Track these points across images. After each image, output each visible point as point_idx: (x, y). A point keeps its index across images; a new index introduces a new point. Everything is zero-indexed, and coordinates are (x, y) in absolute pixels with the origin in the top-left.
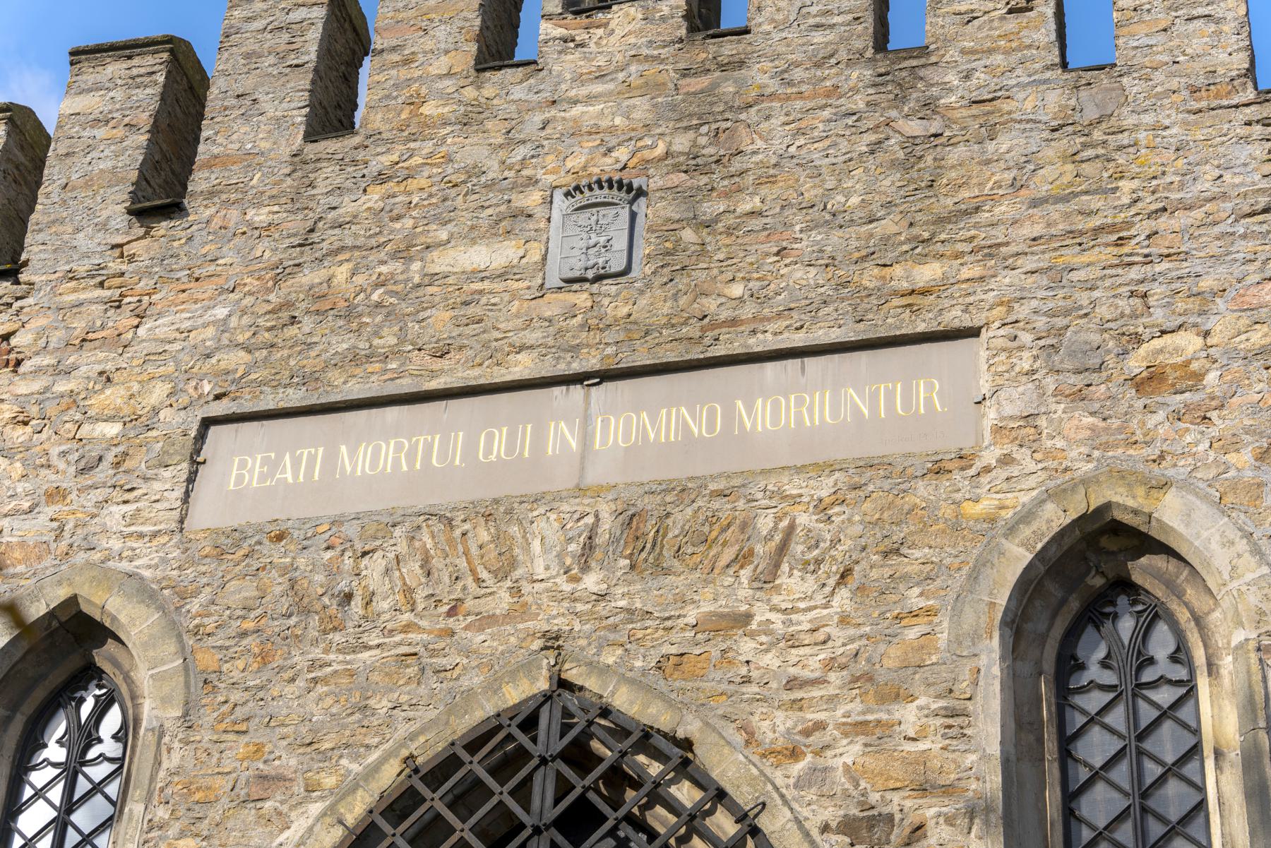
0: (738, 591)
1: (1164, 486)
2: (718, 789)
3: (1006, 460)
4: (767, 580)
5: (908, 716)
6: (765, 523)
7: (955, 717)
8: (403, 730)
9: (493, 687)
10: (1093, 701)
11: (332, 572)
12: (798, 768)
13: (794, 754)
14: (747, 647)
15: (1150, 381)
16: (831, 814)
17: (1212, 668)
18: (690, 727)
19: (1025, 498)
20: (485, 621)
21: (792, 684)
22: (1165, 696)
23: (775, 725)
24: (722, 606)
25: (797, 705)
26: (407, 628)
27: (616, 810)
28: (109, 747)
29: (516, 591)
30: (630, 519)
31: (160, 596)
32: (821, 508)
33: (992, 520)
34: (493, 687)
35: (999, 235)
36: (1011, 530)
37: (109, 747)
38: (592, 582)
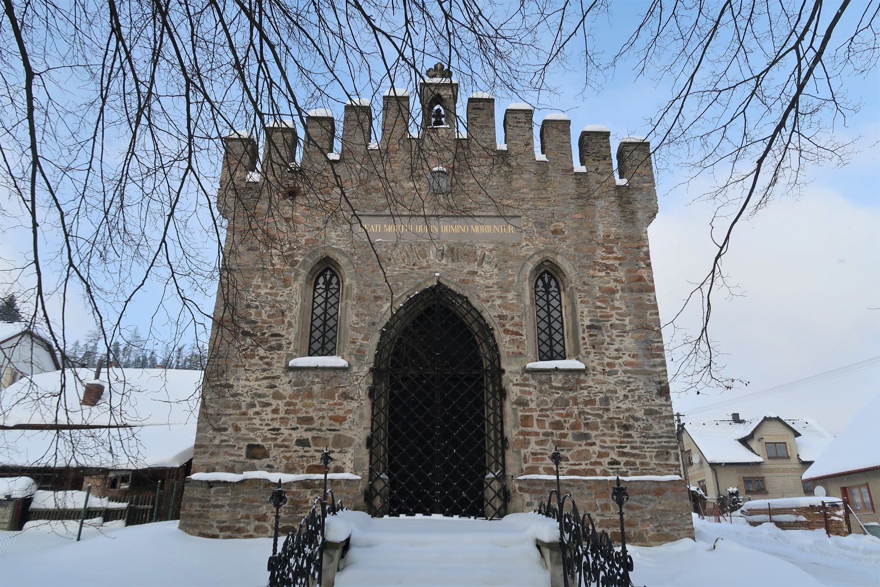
0: (474, 267)
1: (558, 254)
2: (767, 493)
3: (527, 245)
4: (480, 264)
5: (510, 296)
6: (479, 252)
7: (519, 296)
8: (406, 289)
9: (425, 281)
10: (320, 291)
11: (386, 252)
12: (489, 304)
13: (488, 301)
14: (477, 279)
15: (555, 232)
16: (496, 314)
17: (564, 290)
18: (466, 294)
19: (531, 253)
20: (421, 268)
21: (487, 287)
22: (334, 291)
23: (483, 295)
24: (472, 269)
25: (489, 292)
26: (404, 267)
27: (471, 100)
28: (334, 285)
29: (427, 262)
30: (452, 250)
31: (349, 255)
32: (491, 251)
33: (524, 257)
34: (425, 281)
35: (524, 195)
36: (529, 259)
37: (334, 285)
38: (444, 262)
